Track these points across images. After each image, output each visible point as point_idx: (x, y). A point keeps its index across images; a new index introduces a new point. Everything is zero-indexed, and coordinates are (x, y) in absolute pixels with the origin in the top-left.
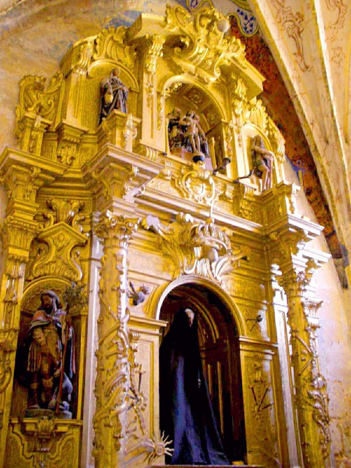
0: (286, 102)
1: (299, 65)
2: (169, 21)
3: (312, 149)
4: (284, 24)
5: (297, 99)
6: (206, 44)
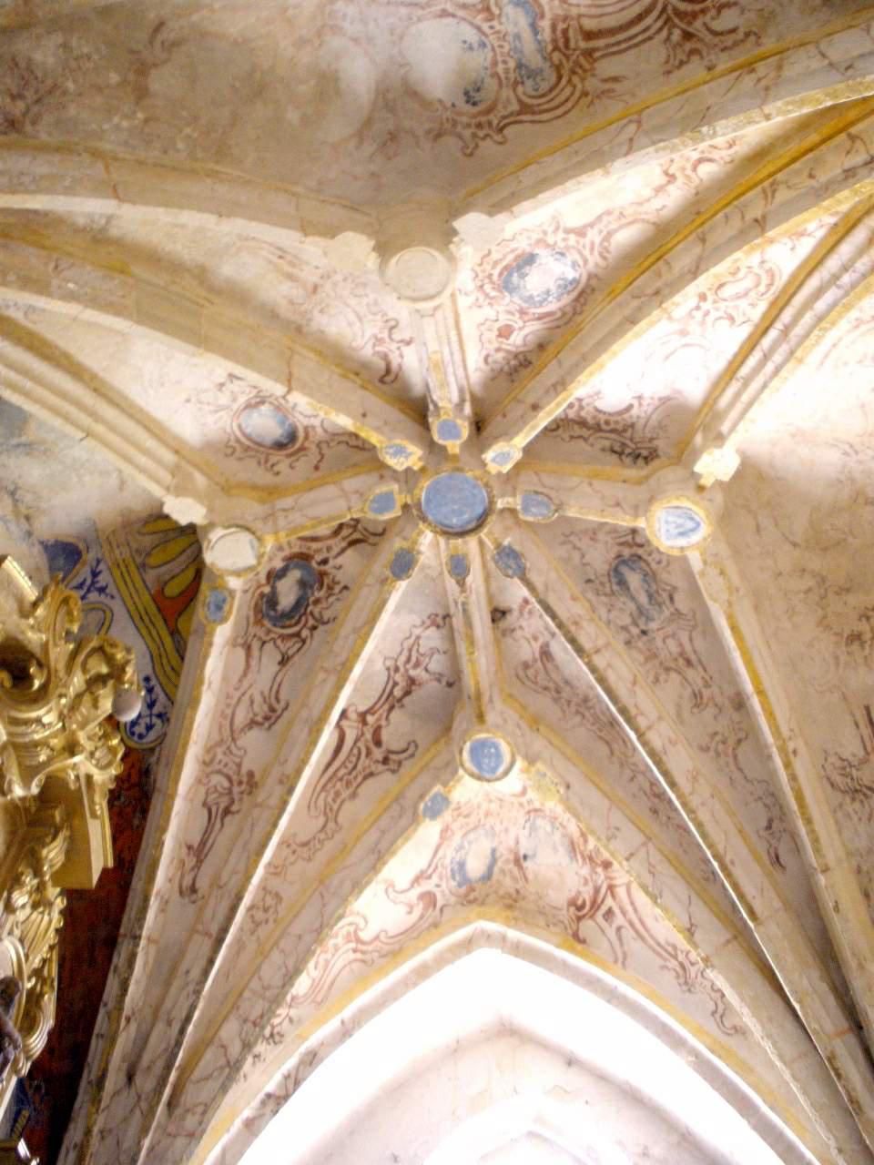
0: (102, 933)
1: (182, 876)
2: (40, 611)
3: (90, 1074)
4: (212, 772)
5: (137, 945)
6: (65, 711)
